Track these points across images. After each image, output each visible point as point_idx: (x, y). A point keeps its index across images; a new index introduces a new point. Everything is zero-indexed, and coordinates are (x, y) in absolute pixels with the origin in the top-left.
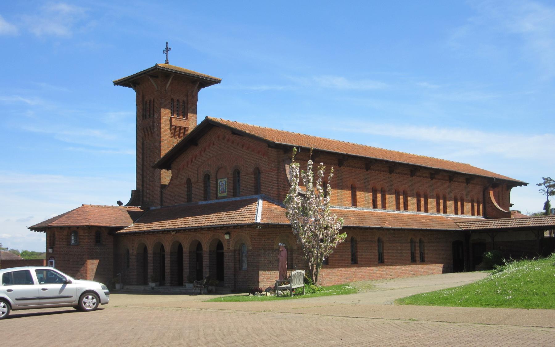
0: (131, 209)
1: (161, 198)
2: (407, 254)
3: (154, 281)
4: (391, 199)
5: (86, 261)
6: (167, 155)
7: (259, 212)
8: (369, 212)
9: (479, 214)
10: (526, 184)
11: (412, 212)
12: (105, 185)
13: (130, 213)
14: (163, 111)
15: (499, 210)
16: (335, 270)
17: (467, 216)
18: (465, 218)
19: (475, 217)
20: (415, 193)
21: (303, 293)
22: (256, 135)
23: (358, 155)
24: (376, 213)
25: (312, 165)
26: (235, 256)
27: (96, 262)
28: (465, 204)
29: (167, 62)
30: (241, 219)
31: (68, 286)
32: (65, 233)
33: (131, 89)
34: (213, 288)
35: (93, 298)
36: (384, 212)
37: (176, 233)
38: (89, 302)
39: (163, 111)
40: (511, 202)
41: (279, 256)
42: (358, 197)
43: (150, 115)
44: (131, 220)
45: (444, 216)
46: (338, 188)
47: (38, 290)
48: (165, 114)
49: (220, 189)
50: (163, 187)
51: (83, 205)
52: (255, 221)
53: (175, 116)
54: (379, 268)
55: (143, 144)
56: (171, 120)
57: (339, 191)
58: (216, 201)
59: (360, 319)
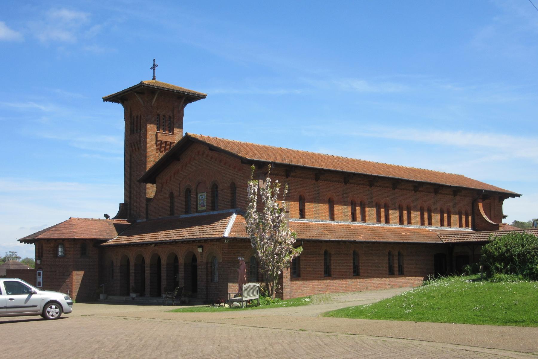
0: (118, 221)
1: (147, 211)
2: (385, 266)
3: (135, 292)
4: (371, 212)
5: (72, 272)
6: (150, 170)
7: (229, 227)
8: (335, 225)
9: (467, 226)
10: (519, 196)
11: (394, 225)
12: (93, 198)
13: (116, 225)
14: (149, 126)
15: (487, 222)
16: (307, 283)
17: (454, 229)
18: (454, 230)
19: (463, 229)
20: (397, 206)
21: (257, 305)
22: (231, 151)
23: (334, 169)
24: (355, 226)
25: (271, 182)
26: (207, 268)
27: (81, 273)
28: (452, 216)
29: (154, 78)
30: (211, 233)
31: (33, 296)
32: (52, 245)
33: (120, 105)
34: (187, 299)
35: (56, 308)
36: (364, 225)
37: (155, 246)
38: (53, 311)
39: (149, 126)
40: (504, 213)
41: (238, 270)
42: (335, 210)
43: (137, 130)
44: (116, 233)
45: (428, 228)
46: (315, 202)
47: (5, 300)
48: (151, 130)
49: (200, 202)
50: (149, 200)
51: (70, 218)
52: (222, 236)
53: (161, 131)
54: (353, 280)
55: (131, 159)
56: (156, 135)
57: (316, 205)
58: (196, 214)
59: (265, 329)
